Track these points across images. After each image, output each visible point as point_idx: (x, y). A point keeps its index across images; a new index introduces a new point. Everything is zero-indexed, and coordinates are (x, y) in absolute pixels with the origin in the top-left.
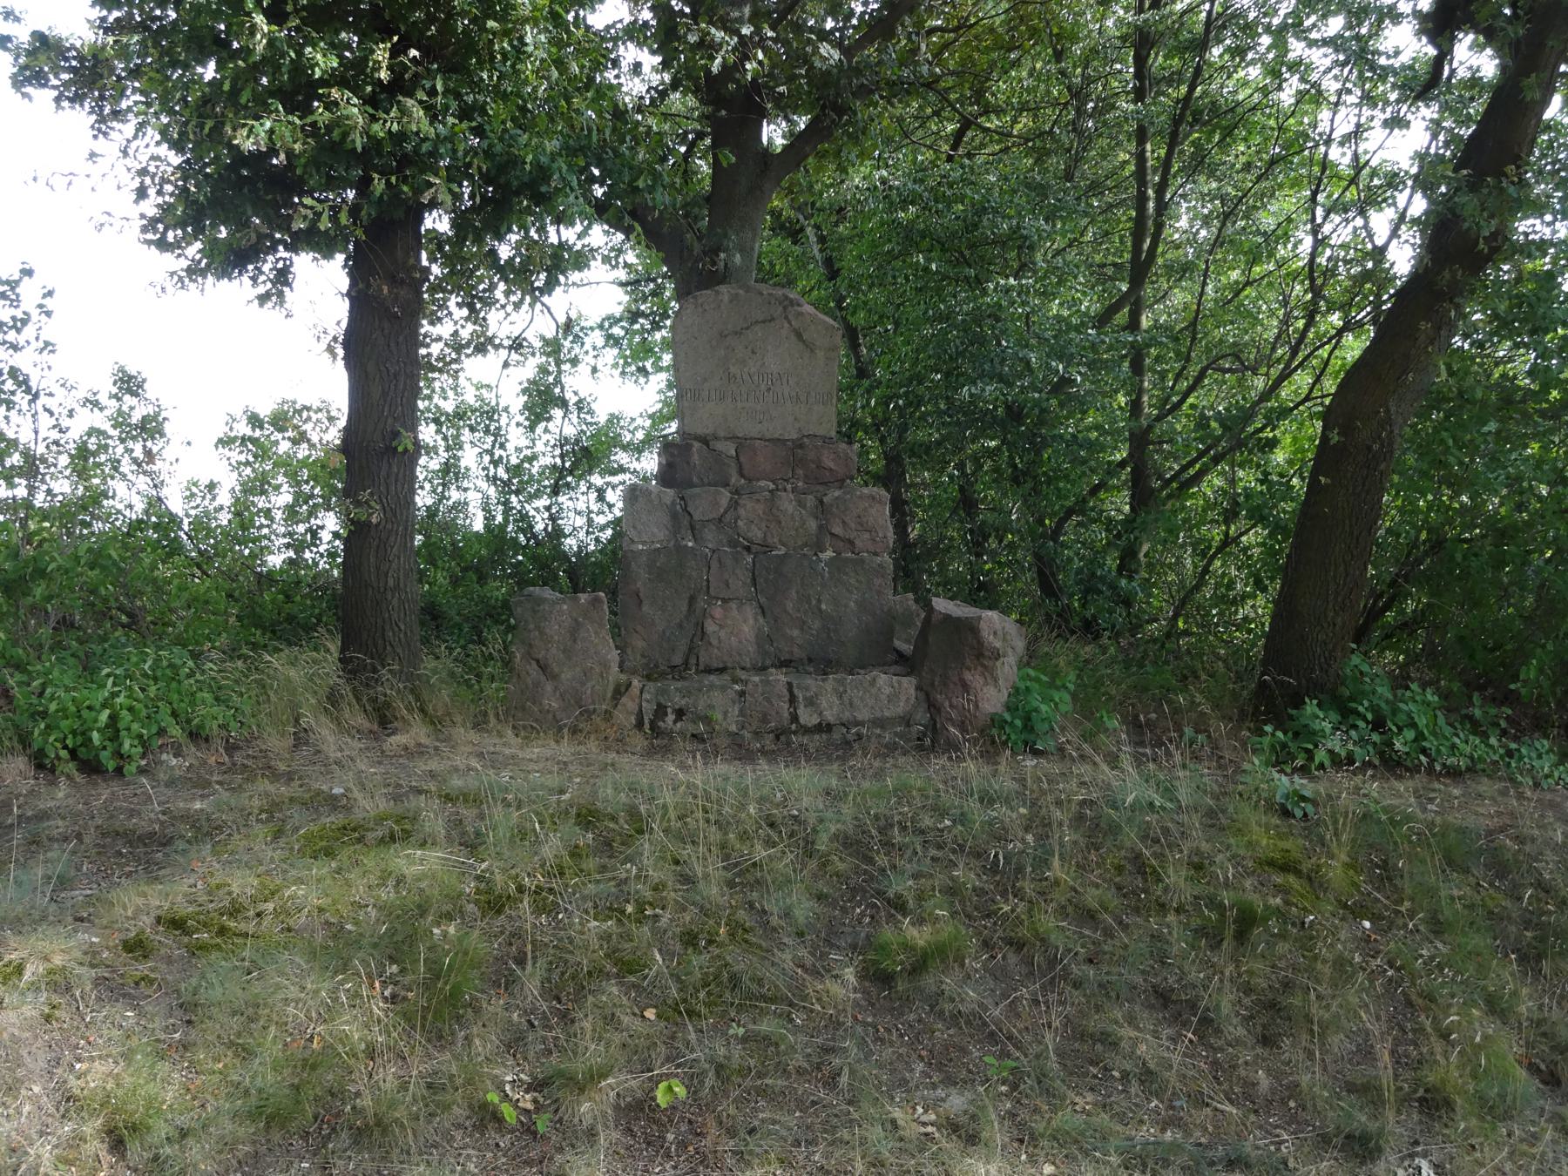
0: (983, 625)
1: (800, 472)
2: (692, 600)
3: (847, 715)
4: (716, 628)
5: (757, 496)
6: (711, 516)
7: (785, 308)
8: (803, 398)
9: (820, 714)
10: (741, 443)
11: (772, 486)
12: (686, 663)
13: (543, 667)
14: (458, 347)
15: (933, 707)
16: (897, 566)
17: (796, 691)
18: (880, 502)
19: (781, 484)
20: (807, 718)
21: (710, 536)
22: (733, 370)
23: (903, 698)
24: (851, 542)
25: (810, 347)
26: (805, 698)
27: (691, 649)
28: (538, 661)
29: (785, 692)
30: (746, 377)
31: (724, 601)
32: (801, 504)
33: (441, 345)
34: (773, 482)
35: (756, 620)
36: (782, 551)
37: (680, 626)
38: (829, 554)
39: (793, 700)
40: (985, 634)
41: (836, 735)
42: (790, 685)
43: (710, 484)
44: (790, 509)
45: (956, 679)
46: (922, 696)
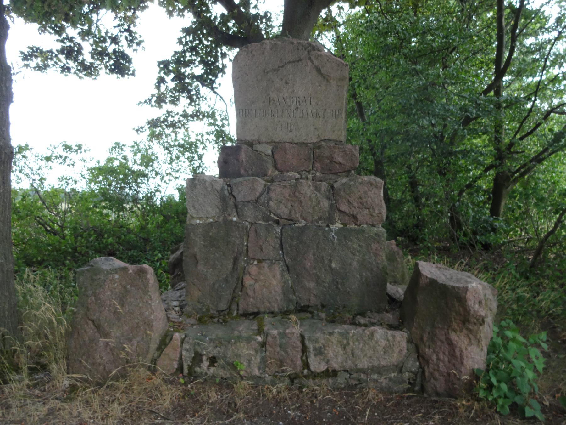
0: (469, 295)
1: (318, 165)
2: (236, 260)
3: (349, 364)
4: (252, 282)
5: (284, 183)
6: (250, 198)
7: (309, 52)
8: (321, 114)
9: (327, 362)
10: (277, 146)
11: (297, 176)
12: (229, 308)
13: (98, 327)
14: (185, 115)
15: (421, 357)
16: (388, 230)
17: (307, 342)
18: (376, 187)
19: (304, 174)
20: (317, 365)
21: (249, 213)
22: (273, 95)
23: (397, 350)
24: (355, 217)
25: (326, 78)
26: (315, 349)
27: (233, 298)
28: (93, 321)
29: (299, 344)
30: (281, 99)
31: (260, 261)
32: (317, 189)
33: (178, 116)
34: (299, 174)
35: (282, 275)
36: (303, 223)
37: (226, 280)
38: (338, 225)
39: (305, 350)
40: (471, 303)
41: (341, 380)
42: (302, 337)
43: (253, 175)
44: (309, 193)
45: (443, 338)
46: (412, 347)
